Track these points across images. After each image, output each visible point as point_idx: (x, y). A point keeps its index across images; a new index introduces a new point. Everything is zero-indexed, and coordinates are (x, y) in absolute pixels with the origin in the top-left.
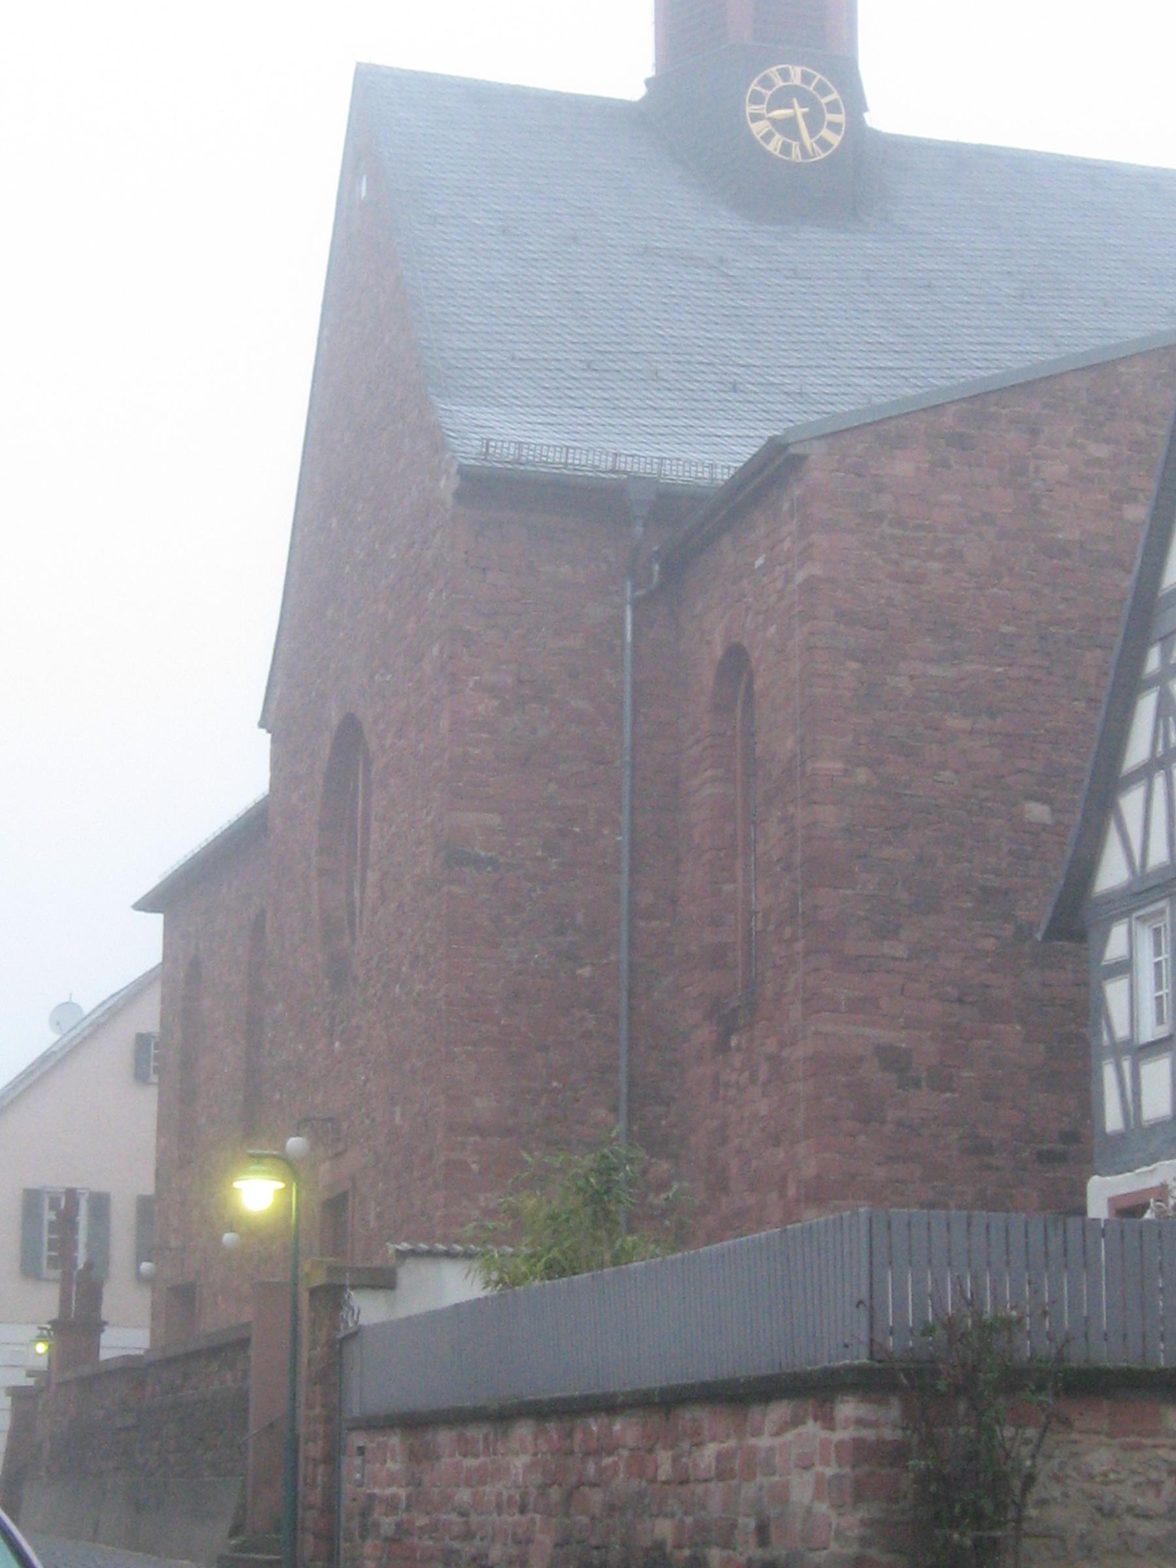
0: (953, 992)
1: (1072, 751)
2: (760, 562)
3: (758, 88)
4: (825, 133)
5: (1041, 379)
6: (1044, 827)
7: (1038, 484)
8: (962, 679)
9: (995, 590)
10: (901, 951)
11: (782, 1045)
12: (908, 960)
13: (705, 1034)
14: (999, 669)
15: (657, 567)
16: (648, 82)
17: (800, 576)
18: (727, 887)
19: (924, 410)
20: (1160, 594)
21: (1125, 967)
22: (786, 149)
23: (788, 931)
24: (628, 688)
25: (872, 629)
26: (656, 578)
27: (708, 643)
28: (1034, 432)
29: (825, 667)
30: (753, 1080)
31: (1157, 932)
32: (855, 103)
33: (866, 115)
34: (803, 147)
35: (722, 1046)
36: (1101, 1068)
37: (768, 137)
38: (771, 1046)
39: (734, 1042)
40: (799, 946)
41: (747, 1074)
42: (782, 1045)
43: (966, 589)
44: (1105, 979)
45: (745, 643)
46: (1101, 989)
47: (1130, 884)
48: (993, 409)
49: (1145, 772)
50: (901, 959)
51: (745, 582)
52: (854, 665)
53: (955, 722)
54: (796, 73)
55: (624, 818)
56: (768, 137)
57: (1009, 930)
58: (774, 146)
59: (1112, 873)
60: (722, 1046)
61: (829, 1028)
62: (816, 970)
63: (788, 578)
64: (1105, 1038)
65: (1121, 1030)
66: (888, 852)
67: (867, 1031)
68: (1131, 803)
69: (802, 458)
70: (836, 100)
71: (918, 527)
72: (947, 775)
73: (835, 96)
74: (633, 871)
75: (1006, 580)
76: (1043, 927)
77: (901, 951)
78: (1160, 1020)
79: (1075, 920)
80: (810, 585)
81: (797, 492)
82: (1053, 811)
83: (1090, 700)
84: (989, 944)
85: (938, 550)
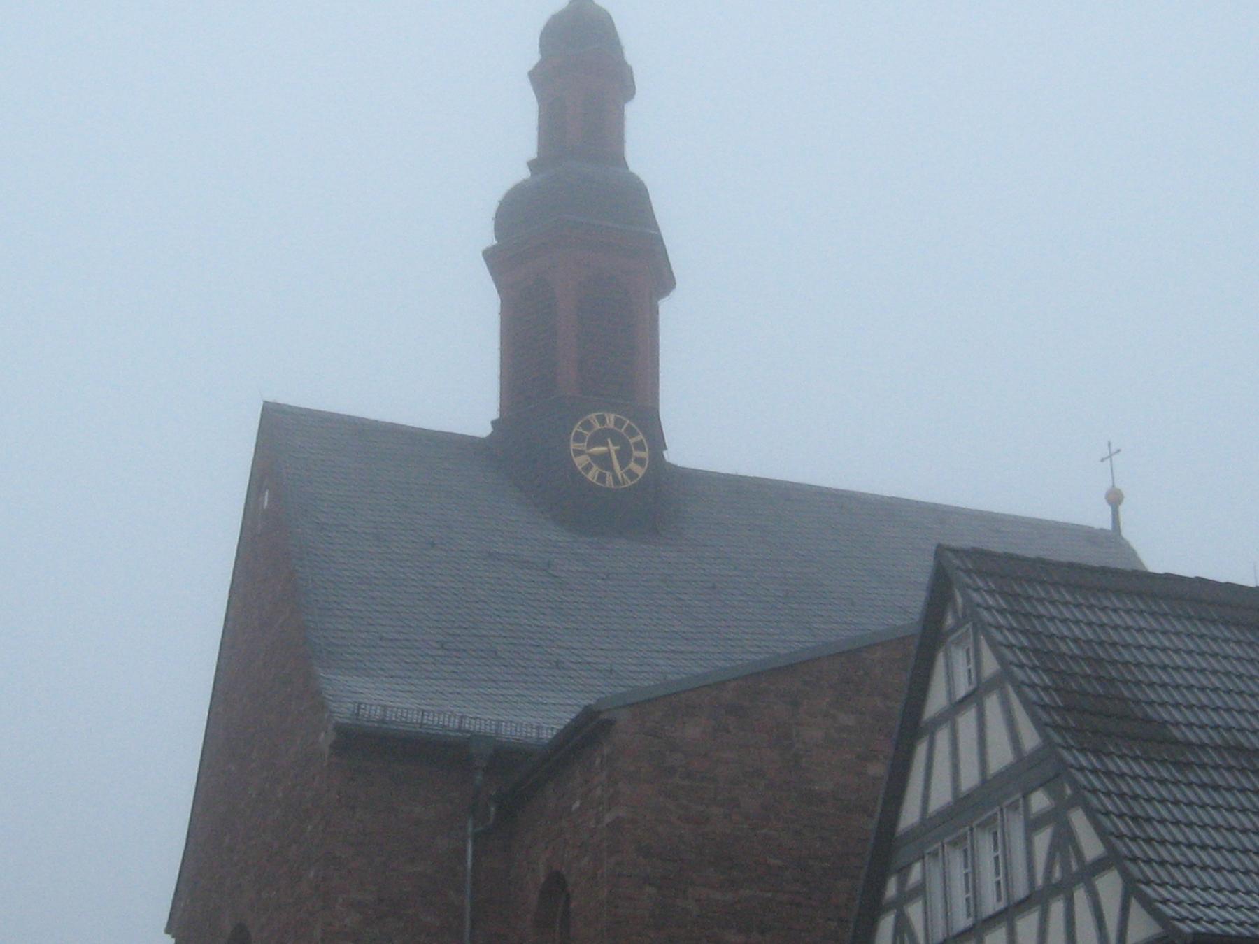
4: (633, 466)
15: (493, 809)
16: (494, 423)
17: (608, 818)
20: (897, 835)
22: (602, 477)
34: (615, 477)
37: (588, 468)
52: (650, 890)
54: (611, 418)
56: (588, 468)
58: (592, 475)
69: (611, 723)
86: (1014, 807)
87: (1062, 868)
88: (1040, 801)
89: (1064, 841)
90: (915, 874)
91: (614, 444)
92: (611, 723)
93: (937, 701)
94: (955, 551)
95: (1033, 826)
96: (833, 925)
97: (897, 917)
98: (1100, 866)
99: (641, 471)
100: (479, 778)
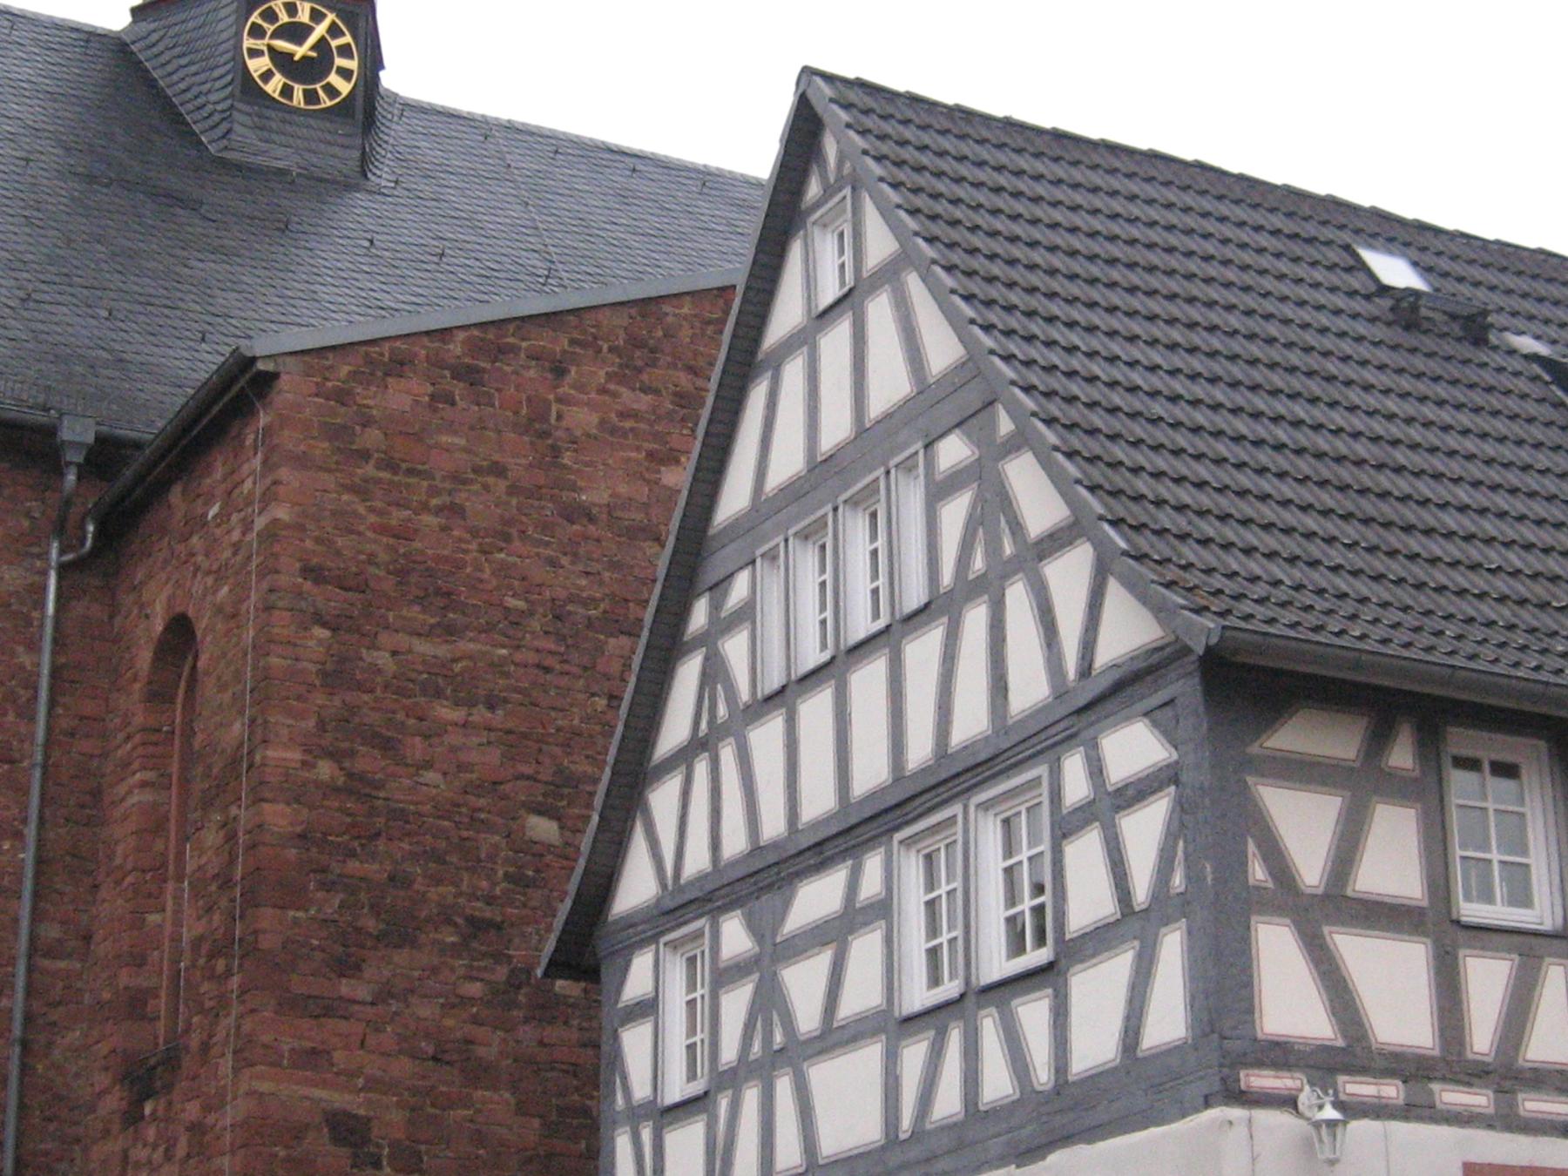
0: (428, 1048)
1: (587, 757)
2: (213, 511)
3: (260, 21)
5: (570, 312)
6: (549, 847)
7: (559, 433)
8: (455, 660)
9: (502, 555)
10: (363, 992)
11: (207, 1109)
12: (372, 1004)
13: (113, 1102)
14: (504, 651)
15: (91, 528)
17: (260, 523)
18: (153, 918)
19: (427, 333)
20: (711, 532)
21: (648, 1008)
23: (220, 965)
24: (45, 671)
25: (345, 589)
26: (89, 543)
27: (147, 617)
28: (560, 371)
29: (285, 632)
30: (168, 1156)
31: (692, 961)
32: (373, 60)
33: (382, 74)
35: (132, 1117)
36: (613, 1139)
37: (267, 76)
38: (192, 1110)
39: (148, 1109)
40: (235, 981)
41: (161, 1149)
42: (207, 1109)
43: (466, 551)
44: (622, 1025)
45: (191, 613)
46: (616, 1037)
47: (659, 900)
48: (511, 340)
49: (684, 756)
50: (363, 1003)
51: (195, 539)
52: (321, 633)
53: (446, 712)
55: (31, 832)
57: (501, 973)
59: (637, 888)
60: (132, 1117)
61: (265, 1087)
62: (253, 1011)
63: (247, 526)
64: (620, 1101)
65: (641, 1090)
66: (353, 865)
67: (318, 1093)
68: (663, 799)
69: (271, 377)
70: (349, 45)
71: (410, 472)
72: (430, 776)
73: (347, 39)
74: (37, 895)
75: (517, 543)
76: (544, 962)
77: (363, 992)
78: (692, 1076)
79: (588, 949)
80: (271, 533)
81: (263, 419)
82: (561, 828)
83: (611, 697)
84: (475, 989)
85: (434, 502)
86: (908, 466)
87: (987, 554)
88: (954, 451)
89: (996, 505)
90: (739, 589)
91: (304, 58)
92: (271, 377)
93: (787, 314)
94: (829, 78)
95: (939, 492)
96: (601, 703)
97: (706, 659)
98: (1055, 542)
99: (344, 88)
100: (71, 477)
